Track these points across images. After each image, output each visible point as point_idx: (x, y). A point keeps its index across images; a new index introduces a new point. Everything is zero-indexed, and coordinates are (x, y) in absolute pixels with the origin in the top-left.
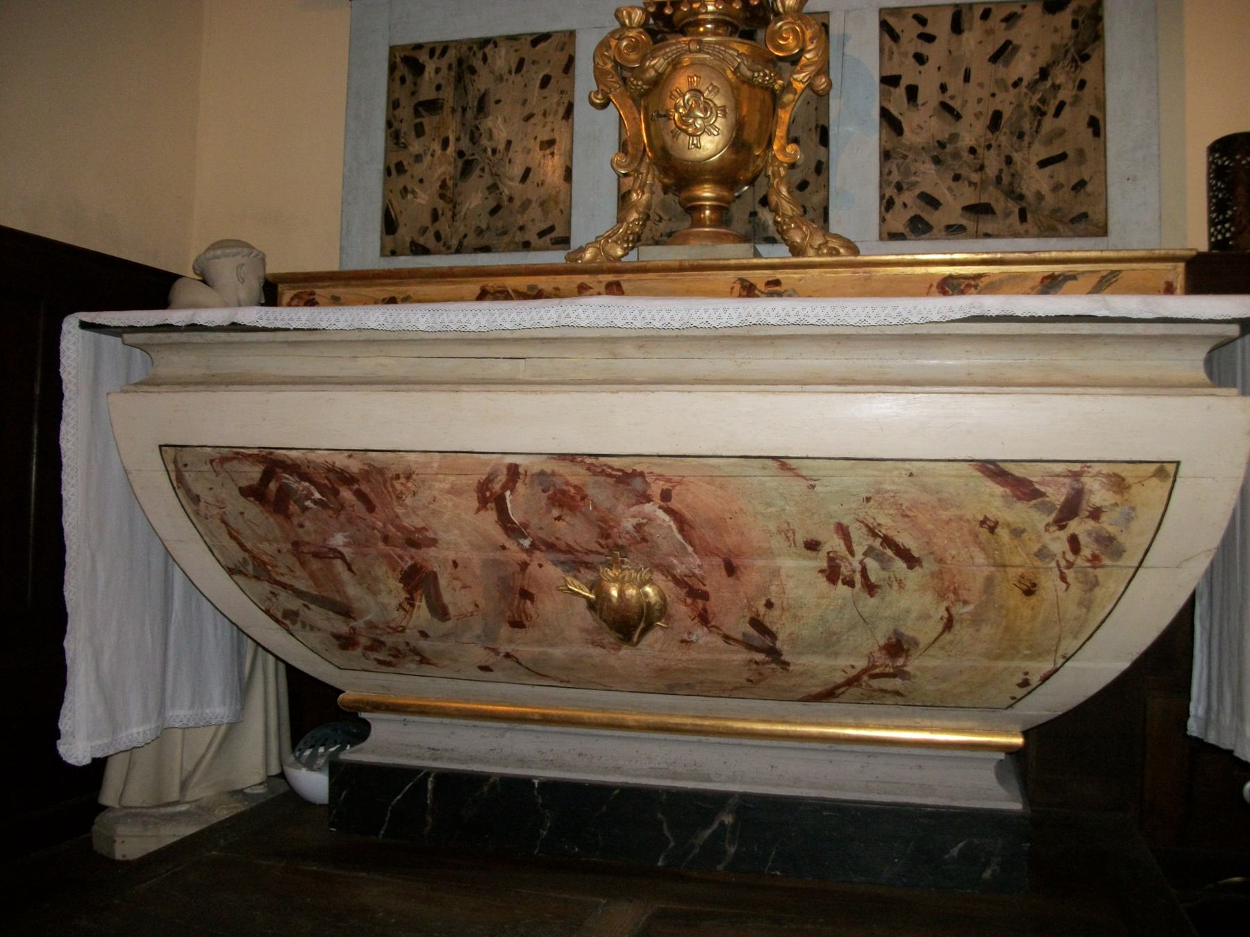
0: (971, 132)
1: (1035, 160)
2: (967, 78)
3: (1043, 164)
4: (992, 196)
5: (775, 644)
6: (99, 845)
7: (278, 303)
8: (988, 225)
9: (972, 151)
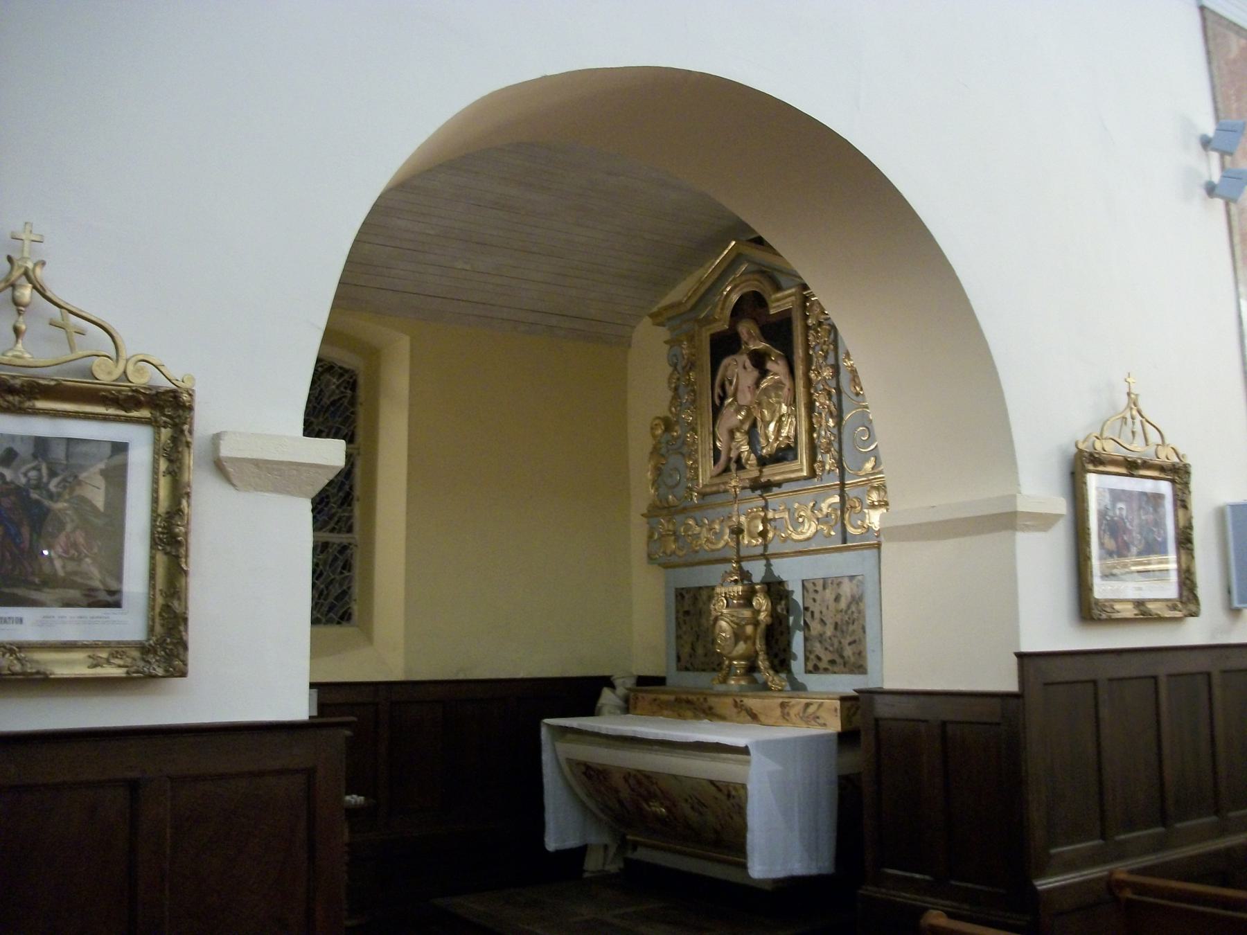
0: (829, 631)
1: (847, 641)
2: (828, 608)
3: (850, 644)
4: (836, 657)
5: (752, 581)
6: (787, 588)
7: (596, 712)
8: (836, 669)
9: (830, 638)
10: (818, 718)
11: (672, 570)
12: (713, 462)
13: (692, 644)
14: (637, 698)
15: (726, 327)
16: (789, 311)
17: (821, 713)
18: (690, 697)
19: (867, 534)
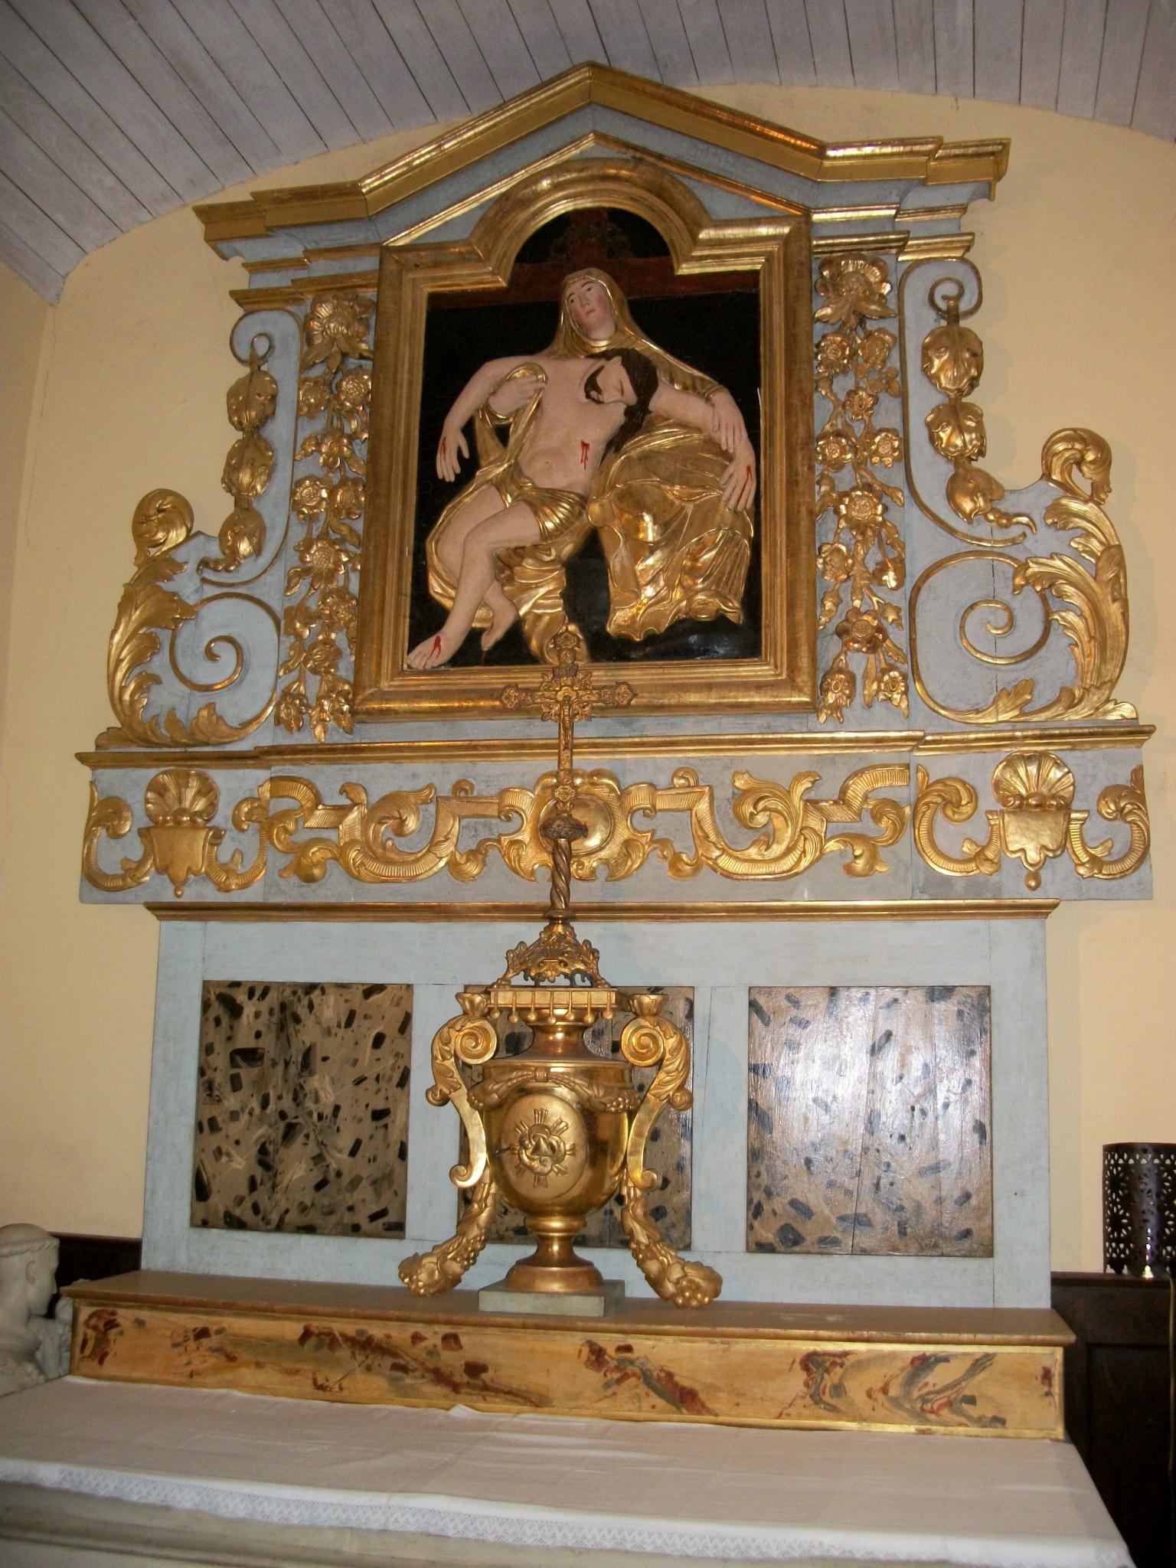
10: (971, 1400)
11: (391, 766)
12: (406, 645)
13: (263, 1150)
14: (111, 1324)
15: (503, 283)
16: (757, 272)
17: (979, 1384)
18: (376, 1331)
19: (995, 878)
